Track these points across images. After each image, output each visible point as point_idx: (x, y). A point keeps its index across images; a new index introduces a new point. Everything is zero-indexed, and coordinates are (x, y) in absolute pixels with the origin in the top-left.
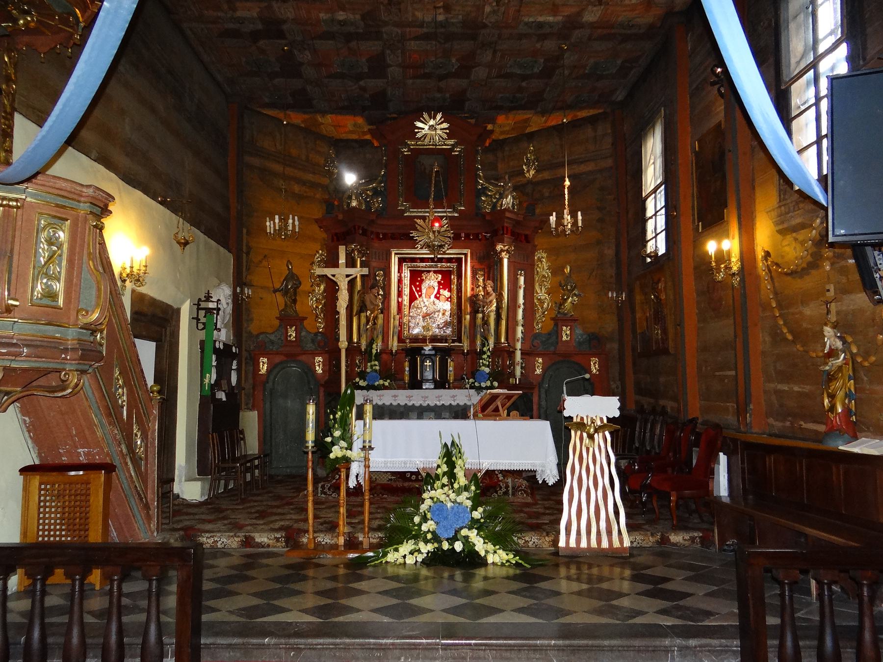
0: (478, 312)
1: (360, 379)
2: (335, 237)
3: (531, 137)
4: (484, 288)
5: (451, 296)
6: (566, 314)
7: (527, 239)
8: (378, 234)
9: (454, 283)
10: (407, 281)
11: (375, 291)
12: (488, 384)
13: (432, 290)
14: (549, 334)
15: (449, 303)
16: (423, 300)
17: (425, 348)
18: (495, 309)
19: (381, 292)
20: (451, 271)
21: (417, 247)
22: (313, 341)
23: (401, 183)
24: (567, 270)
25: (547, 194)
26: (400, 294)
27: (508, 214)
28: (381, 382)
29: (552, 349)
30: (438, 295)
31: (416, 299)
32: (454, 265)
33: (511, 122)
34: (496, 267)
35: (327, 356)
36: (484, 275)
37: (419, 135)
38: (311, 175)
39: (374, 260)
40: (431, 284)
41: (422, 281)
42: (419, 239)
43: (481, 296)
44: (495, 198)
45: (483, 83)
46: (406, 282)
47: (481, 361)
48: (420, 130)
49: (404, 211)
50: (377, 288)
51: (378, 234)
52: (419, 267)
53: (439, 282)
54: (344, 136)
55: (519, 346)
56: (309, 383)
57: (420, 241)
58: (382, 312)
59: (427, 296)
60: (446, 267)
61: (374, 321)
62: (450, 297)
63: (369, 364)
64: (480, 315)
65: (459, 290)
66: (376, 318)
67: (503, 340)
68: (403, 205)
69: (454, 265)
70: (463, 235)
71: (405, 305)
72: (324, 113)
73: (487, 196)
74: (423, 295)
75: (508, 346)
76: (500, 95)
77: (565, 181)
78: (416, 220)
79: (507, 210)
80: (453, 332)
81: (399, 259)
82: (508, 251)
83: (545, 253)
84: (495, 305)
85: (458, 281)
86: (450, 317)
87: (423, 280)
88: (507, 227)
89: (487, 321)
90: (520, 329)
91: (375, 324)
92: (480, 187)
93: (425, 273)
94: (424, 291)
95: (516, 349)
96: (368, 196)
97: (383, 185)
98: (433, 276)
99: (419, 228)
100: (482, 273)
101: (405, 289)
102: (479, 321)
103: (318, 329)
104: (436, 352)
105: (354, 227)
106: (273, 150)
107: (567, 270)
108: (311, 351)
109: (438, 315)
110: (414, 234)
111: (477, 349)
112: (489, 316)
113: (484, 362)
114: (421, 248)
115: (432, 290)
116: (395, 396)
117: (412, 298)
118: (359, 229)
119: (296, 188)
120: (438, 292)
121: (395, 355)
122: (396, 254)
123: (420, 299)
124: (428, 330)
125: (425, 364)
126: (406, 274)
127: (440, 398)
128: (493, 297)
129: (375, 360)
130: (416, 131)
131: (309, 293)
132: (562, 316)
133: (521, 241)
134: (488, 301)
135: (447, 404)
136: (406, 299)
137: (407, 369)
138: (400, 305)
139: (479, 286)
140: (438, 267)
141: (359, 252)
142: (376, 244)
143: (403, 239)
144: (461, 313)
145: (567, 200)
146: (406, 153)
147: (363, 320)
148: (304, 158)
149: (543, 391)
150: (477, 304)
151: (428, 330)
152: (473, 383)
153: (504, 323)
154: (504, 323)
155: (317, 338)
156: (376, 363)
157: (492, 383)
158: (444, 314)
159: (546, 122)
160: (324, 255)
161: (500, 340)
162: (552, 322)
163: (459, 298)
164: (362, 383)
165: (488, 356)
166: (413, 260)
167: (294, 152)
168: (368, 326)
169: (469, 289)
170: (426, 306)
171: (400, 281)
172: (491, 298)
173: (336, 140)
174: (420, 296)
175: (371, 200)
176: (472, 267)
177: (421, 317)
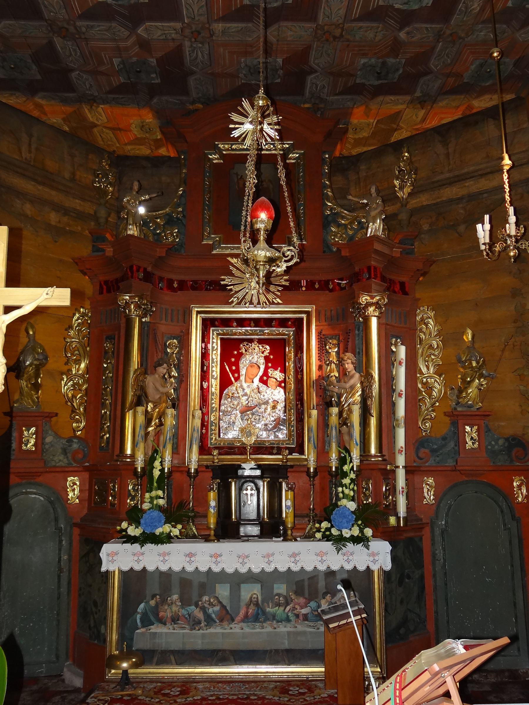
0: (329, 404)
1: (130, 524)
2: (105, 287)
3: (398, 147)
4: (341, 363)
5: (285, 379)
6: (470, 406)
7: (403, 289)
8: (170, 282)
9: (290, 359)
10: (215, 356)
11: (162, 370)
12: (356, 532)
13: (255, 370)
14: (444, 438)
15: (282, 391)
16: (241, 386)
17: (244, 465)
18: (359, 399)
19: (174, 373)
20: (285, 339)
21: (232, 302)
22: (65, 452)
23: (207, 205)
24: (468, 336)
25: (426, 227)
26: (205, 375)
27: (377, 246)
28: (167, 528)
29: (450, 463)
30: (265, 378)
31: (231, 383)
32: (290, 332)
33: (372, 121)
34: (357, 332)
35: (86, 475)
36: (338, 345)
37: (236, 134)
38: (77, 201)
39: (163, 321)
40: (255, 361)
41: (240, 355)
42: (236, 288)
43: (334, 378)
44: (352, 229)
45: (338, 32)
46: (214, 357)
47: (340, 489)
48: (237, 126)
49: (211, 247)
50: (165, 365)
51: (170, 282)
52: (235, 334)
53: (266, 358)
54: (131, 150)
55: (401, 460)
56: (56, 520)
57: (237, 292)
58: (174, 406)
59: (248, 379)
60: (277, 335)
61: (160, 421)
62: (284, 381)
63: (147, 495)
64: (335, 410)
65: (299, 370)
66: (162, 415)
67: (373, 451)
68: (209, 238)
69: (290, 332)
70: (304, 283)
71: (213, 394)
72: (93, 101)
73: (339, 225)
74: (242, 378)
75: (384, 460)
76: (363, 61)
77: (502, 159)
78: (229, 259)
79: (374, 237)
80: (290, 435)
81: (204, 320)
82: (377, 305)
83: (433, 310)
84: (360, 393)
85: (296, 355)
86: (285, 412)
87: (242, 354)
88: (375, 268)
89: (346, 419)
90: (401, 434)
91: (161, 424)
92: (329, 212)
93: (245, 343)
94: (243, 372)
95: (398, 467)
96: (158, 225)
97: (180, 209)
98: (257, 348)
99: (234, 271)
100: (335, 342)
101: (214, 369)
102: (334, 420)
103: (74, 431)
104: (262, 473)
105: (131, 267)
106: (17, 158)
107: (468, 336)
108: (62, 467)
109: (266, 409)
110: (227, 281)
111: (331, 468)
112: (350, 411)
113: (347, 491)
114: (239, 303)
115: (255, 370)
116: (190, 555)
117: (225, 383)
118: (138, 271)
119: (53, 218)
120: (266, 373)
121: (195, 477)
122: (198, 312)
123: (237, 384)
124: (249, 434)
125: (245, 492)
126: (214, 345)
127: (271, 559)
128: (356, 380)
129: (159, 488)
130: (232, 126)
131: (62, 374)
132: (465, 409)
133: (395, 292)
134: (348, 385)
135: (282, 569)
136: (215, 384)
137: (213, 503)
138: (204, 393)
139: (331, 362)
140: (264, 334)
141: (138, 307)
142: (168, 297)
143: (210, 290)
144: (302, 405)
145: (507, 194)
146: (215, 162)
147: (141, 419)
148: (67, 175)
149: (437, 532)
150: (328, 390)
151: (249, 434)
152: (328, 529)
153: (373, 422)
154: (373, 422)
155: (70, 446)
156: (160, 493)
157: (361, 531)
158: (274, 407)
159: (424, 120)
160: (87, 315)
161: (369, 451)
162: (447, 419)
163: (299, 382)
164: (133, 531)
165: (352, 480)
166: (226, 323)
167: (51, 165)
168: (150, 429)
169: (314, 368)
170: (246, 395)
171: (205, 355)
172: (352, 382)
173: (118, 156)
174: (237, 379)
175: (163, 231)
176: (319, 334)
177: (238, 412)
